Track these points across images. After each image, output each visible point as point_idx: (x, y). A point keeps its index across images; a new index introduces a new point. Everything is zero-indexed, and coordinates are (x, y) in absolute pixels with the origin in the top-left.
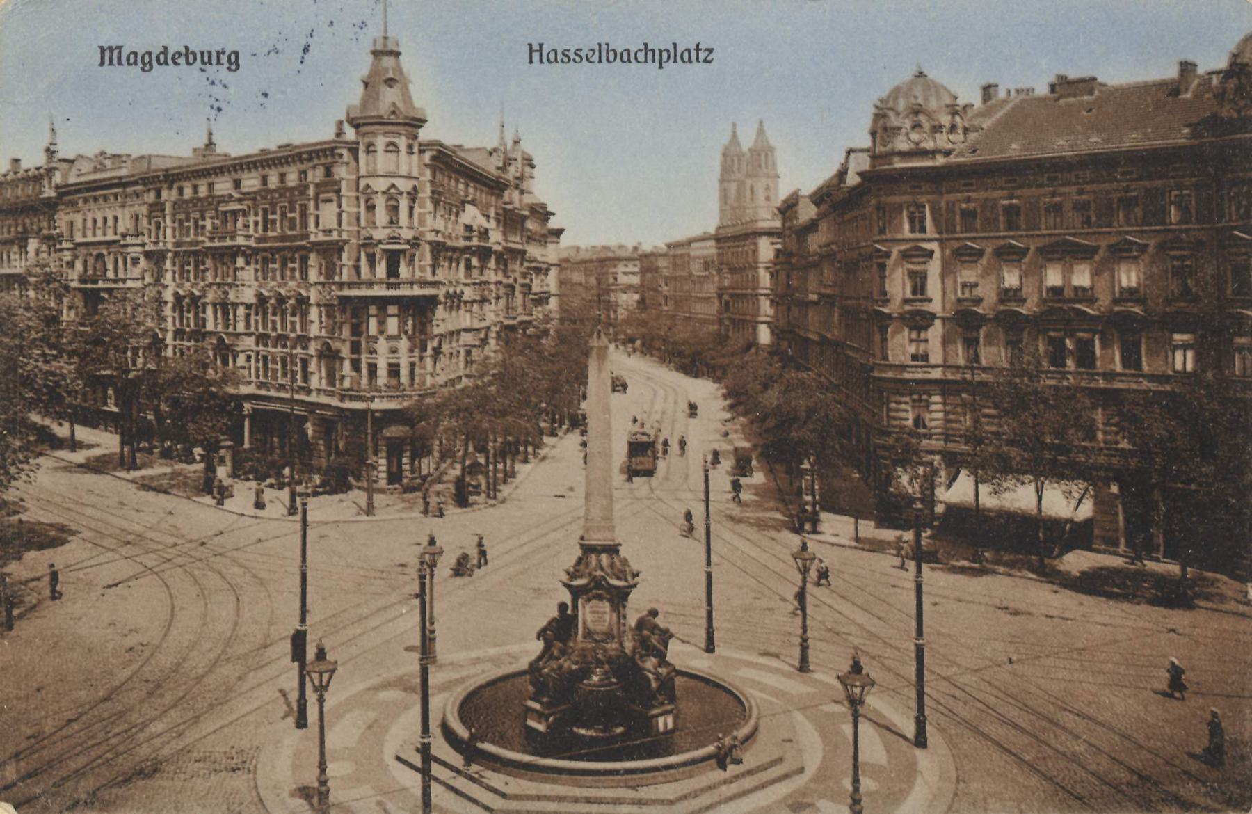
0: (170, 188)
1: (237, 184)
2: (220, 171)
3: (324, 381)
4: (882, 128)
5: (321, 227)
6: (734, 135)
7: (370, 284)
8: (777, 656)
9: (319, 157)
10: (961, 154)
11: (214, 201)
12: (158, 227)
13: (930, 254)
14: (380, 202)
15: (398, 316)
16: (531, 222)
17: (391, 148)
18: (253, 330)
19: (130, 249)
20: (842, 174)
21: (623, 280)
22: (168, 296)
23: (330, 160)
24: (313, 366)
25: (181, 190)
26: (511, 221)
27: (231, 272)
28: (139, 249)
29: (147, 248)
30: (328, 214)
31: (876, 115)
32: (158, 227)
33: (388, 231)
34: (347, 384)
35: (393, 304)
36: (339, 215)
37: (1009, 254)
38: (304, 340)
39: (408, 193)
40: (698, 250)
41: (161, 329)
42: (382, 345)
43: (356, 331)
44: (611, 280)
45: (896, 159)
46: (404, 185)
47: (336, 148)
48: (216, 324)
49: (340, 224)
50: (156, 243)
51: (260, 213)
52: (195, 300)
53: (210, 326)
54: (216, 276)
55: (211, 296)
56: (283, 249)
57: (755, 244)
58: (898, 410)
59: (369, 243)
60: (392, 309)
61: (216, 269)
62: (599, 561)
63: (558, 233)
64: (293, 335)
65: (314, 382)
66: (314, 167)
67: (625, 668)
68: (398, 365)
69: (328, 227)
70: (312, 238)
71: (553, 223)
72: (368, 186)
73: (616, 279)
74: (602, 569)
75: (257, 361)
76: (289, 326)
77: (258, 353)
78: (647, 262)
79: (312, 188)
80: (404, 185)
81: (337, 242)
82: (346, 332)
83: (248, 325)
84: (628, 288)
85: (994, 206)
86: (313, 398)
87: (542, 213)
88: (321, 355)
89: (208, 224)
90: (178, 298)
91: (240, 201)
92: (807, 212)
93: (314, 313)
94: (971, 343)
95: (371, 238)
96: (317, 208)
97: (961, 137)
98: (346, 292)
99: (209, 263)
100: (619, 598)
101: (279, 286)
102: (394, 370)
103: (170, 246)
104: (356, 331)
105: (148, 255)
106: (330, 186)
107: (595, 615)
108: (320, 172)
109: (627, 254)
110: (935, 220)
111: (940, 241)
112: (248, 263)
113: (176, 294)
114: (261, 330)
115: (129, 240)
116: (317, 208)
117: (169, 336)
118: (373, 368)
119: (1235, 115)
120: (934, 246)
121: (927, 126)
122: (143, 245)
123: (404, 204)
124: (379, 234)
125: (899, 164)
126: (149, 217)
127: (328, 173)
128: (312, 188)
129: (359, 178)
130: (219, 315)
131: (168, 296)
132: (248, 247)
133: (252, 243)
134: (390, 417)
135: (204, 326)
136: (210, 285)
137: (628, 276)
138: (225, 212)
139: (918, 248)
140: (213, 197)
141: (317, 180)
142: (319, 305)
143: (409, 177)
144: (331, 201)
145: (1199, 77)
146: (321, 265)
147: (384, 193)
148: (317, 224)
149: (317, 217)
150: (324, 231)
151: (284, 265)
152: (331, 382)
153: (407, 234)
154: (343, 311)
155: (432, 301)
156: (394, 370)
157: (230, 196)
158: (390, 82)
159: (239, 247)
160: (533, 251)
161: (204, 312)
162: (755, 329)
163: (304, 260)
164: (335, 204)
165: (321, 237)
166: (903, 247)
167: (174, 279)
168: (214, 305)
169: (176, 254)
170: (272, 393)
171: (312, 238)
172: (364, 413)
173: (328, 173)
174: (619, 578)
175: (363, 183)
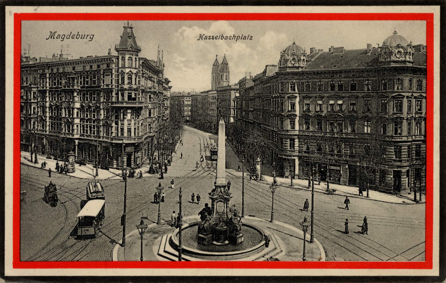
0: (48, 69)
1: (74, 69)
2: (62, 64)
3: (105, 134)
4: (283, 60)
5: (105, 84)
6: (216, 60)
7: (122, 103)
8: (254, 216)
9: (105, 61)
10: (306, 68)
11: (65, 74)
12: (43, 82)
13: (296, 97)
14: (126, 77)
15: (131, 113)
16: (165, 83)
17: (130, 59)
18: (79, 116)
19: (33, 89)
20: (265, 72)
21: (186, 103)
22: (48, 105)
23: (109, 62)
24: (101, 129)
25: (52, 70)
26: (160, 82)
27: (72, 97)
28: (36, 89)
29: (39, 89)
30: (107, 80)
31: (281, 55)
32: (43, 82)
33: (129, 85)
34: (114, 135)
35: (129, 109)
36: (112, 80)
37: (307, 98)
38: (98, 120)
39: (135, 74)
40: (211, 94)
41: (44, 116)
42: (126, 122)
43: (117, 117)
44: (182, 103)
45: (288, 69)
46: (134, 71)
47: (112, 58)
48: (66, 115)
49: (112, 83)
50: (43, 87)
51: (82, 78)
52: (57, 107)
53: (63, 115)
54: (66, 99)
55: (64, 105)
56: (90, 90)
57: (230, 93)
58: (286, 144)
59: (123, 90)
60: (129, 111)
61: (66, 97)
62: (221, 190)
63: (170, 88)
64: (94, 119)
65: (101, 134)
66: (103, 64)
67: (229, 222)
68: (130, 129)
69: (107, 84)
70: (102, 87)
71: (170, 85)
72: (122, 71)
73: (183, 102)
74: (222, 193)
75: (81, 127)
76: (92, 116)
77: (81, 124)
78: (194, 97)
79: (102, 70)
80: (134, 71)
81: (111, 89)
82: (114, 118)
83: (77, 116)
84: (187, 105)
85: (315, 84)
86: (101, 139)
87: (167, 82)
88: (104, 125)
89: (64, 82)
90: (51, 106)
91: (75, 74)
92: (250, 84)
93: (102, 112)
94: (307, 123)
95: (123, 88)
96: (104, 77)
97: (306, 63)
98: (114, 105)
99: (63, 94)
100: (226, 201)
101: (89, 102)
102: (129, 130)
103: (48, 88)
104: (117, 117)
105: (39, 91)
106: (108, 71)
107: (220, 207)
108: (105, 66)
109: (186, 95)
110: (298, 89)
111: (299, 94)
112: (78, 95)
113: (50, 104)
114: (82, 117)
115: (32, 86)
116: (104, 77)
117: (48, 118)
118: (122, 129)
119: (384, 60)
120: (297, 95)
121: (296, 59)
122: (38, 88)
123: (134, 77)
124: (126, 86)
125: (288, 70)
126: (40, 78)
127: (108, 66)
128: (102, 70)
129: (118, 69)
130: (67, 112)
131: (48, 105)
132: (78, 90)
133: (80, 88)
134: (127, 145)
135: (61, 115)
136: (64, 102)
137: (188, 102)
138: (69, 78)
139: (293, 96)
140: (65, 72)
141: (104, 68)
142: (103, 109)
143: (135, 68)
144: (109, 75)
145: (129, 45)
146: (104, 96)
147: (127, 73)
148: (104, 83)
149: (104, 80)
150: (106, 85)
151: (91, 95)
152: (108, 134)
153: (134, 87)
154: (112, 111)
155: (141, 108)
156: (129, 130)
157: (72, 72)
158: (129, 37)
159: (75, 89)
160: (165, 93)
161: (61, 110)
162: (229, 118)
163: (98, 95)
164: (110, 76)
165: (105, 87)
166: (289, 95)
167: (49, 100)
168: (65, 108)
169: (50, 91)
170: (86, 138)
171: (102, 87)
172: (122, 144)
173: (108, 66)
174: (227, 195)
175: (120, 70)
